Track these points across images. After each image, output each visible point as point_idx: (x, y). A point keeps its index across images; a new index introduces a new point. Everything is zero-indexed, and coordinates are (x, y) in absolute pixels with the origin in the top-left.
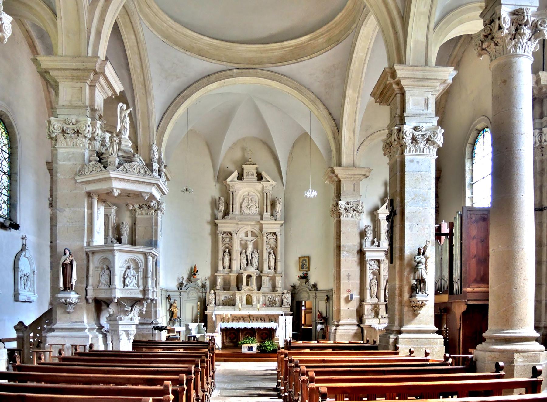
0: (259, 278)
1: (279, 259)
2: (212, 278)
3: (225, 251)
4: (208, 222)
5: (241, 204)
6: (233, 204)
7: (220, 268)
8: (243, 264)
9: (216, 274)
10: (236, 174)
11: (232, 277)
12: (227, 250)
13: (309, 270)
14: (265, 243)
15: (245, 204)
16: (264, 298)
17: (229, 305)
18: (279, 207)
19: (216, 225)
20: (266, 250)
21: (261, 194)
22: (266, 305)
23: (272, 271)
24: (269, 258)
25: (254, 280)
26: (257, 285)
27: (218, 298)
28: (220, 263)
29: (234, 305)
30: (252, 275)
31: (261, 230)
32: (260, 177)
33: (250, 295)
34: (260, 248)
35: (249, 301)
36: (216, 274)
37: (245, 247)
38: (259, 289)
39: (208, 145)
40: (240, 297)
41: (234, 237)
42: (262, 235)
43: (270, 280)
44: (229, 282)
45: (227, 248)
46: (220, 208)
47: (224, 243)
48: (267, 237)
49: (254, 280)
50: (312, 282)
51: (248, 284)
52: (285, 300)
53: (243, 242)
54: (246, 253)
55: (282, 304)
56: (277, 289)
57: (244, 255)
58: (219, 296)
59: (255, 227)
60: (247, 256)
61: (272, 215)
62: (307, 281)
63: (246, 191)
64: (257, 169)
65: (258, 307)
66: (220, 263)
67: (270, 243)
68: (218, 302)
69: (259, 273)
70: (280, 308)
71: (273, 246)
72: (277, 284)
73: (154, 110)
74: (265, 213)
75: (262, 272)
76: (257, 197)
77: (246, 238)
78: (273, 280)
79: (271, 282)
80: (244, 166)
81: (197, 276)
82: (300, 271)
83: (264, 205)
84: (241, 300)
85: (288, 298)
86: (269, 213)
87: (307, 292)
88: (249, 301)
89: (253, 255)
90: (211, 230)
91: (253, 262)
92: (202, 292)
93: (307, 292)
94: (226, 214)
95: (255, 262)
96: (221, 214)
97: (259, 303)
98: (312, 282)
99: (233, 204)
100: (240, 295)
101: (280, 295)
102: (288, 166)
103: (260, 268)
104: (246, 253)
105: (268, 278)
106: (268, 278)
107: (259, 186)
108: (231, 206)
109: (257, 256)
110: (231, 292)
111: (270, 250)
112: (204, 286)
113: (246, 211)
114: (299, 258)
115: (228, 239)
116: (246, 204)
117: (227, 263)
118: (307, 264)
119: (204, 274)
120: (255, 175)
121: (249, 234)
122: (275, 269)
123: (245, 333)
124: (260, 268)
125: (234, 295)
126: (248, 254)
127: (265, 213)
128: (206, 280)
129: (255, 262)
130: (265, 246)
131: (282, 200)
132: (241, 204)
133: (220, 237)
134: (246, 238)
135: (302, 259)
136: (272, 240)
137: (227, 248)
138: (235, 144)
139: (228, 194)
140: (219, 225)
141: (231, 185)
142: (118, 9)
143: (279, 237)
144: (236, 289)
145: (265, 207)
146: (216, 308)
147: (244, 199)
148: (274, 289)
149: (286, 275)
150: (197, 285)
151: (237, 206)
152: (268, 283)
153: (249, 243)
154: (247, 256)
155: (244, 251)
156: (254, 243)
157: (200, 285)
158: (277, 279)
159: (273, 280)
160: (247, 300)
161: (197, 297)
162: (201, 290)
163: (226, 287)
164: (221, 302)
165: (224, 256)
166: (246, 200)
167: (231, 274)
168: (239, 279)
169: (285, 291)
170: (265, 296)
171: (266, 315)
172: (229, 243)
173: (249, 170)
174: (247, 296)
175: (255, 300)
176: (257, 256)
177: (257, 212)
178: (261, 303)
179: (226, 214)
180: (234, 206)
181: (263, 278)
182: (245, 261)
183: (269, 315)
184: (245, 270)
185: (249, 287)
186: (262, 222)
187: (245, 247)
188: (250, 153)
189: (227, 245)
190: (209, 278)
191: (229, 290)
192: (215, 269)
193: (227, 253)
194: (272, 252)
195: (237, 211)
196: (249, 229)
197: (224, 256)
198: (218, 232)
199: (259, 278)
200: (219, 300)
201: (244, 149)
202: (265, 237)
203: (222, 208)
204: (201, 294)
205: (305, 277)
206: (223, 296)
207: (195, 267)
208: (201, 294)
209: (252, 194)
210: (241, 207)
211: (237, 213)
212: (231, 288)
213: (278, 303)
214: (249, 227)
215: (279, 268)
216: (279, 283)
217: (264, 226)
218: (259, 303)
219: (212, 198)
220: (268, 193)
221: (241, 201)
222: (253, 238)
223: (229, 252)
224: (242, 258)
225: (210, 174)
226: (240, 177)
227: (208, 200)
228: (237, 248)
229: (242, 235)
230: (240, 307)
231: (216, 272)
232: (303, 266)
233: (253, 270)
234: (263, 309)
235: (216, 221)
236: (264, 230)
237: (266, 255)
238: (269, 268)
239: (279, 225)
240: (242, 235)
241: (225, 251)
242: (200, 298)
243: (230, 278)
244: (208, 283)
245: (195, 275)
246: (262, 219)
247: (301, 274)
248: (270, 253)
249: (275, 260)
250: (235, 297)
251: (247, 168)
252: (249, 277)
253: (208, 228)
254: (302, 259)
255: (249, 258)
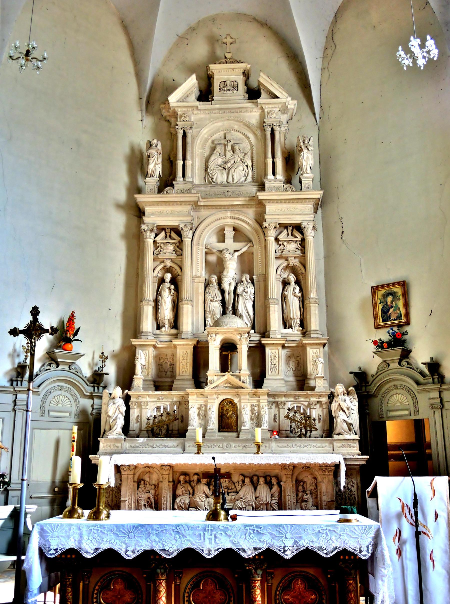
0: (258, 352)
1: (312, 294)
2: (126, 355)
3: (162, 281)
4: (119, 206)
5: (207, 161)
6: (184, 159)
7: (148, 324)
8: (213, 314)
9: (135, 342)
10: (191, 83)
11: (180, 352)
12: (168, 276)
13: (408, 323)
14: (272, 256)
15: (216, 160)
16: (274, 410)
17: (169, 434)
18: (307, 160)
19: (140, 213)
20: (275, 274)
21: (259, 133)
22: (278, 433)
23: (295, 332)
24: (284, 297)
25: (242, 357)
26: (253, 375)
27: (134, 413)
28: (148, 311)
29: (181, 433)
30: (236, 338)
31: (260, 220)
32: (253, 94)
33: (231, 402)
34: (258, 270)
35: (228, 422)
36: (135, 342)
37: (217, 268)
38: (258, 382)
39: (125, 28)
40: (203, 407)
41: (187, 241)
42: (264, 230)
43: (289, 357)
44: (173, 366)
45: (168, 270)
46: (151, 167)
47: (161, 256)
48: (277, 240)
49: (242, 357)
50: (421, 356)
51: (224, 368)
52: (341, 417)
53: (213, 258)
54: (219, 284)
55: (329, 431)
56: (312, 383)
57: (214, 290)
58: (139, 405)
59: (245, 214)
60: (222, 292)
61: (288, 181)
62: (406, 354)
63: (218, 131)
64: (246, 75)
65: (259, 439)
66: (148, 311)
67: (285, 253)
68: (134, 425)
69: (256, 338)
70: (325, 444)
71: (294, 262)
72: (310, 368)
73: (250, 471)
74: (270, 176)
75: (265, 333)
76: (248, 141)
77: (221, 246)
78: (298, 358)
79: (292, 365)
80: (212, 66)
81: (76, 347)
82: (377, 327)
83: (265, 157)
84: (204, 416)
85: (348, 410)
86: (280, 176)
87: (409, 391)
88: (228, 422)
89: (240, 290)
90: (128, 227)
91: (241, 308)
92: (91, 397)
93: (409, 391)
94: (167, 182)
95: (245, 305)
96: (152, 182)
97: (259, 425)
98: (421, 356)
99: (184, 159)
100: (201, 401)
101: (324, 399)
102: (323, 69)
103: (261, 326)
104: (219, 284)
105: (283, 353)
106: (283, 353)
107: (252, 114)
108: (180, 163)
109: (251, 290)
110: (175, 395)
111: (285, 275)
112: (97, 378)
113: (220, 177)
114: (374, 289)
115: (171, 248)
116: (220, 161)
117: (166, 312)
118: (401, 304)
119: (97, 344)
120: (242, 88)
121: (229, 234)
122: (302, 324)
123: (186, 580)
124: (261, 326)
125: (183, 403)
126: (225, 286)
127: (270, 176)
128: (104, 358)
129: (245, 305)
130: (273, 264)
131: (313, 142)
132: (207, 161)
133: (150, 241)
134: (221, 246)
135: (383, 291)
136: (292, 247)
137: (168, 270)
138: (192, 29)
139: (173, 136)
140: (148, 210)
141: (180, 112)
142: (329, 521)
143: (310, 234)
144: (191, 383)
145: (270, 161)
146: (127, 444)
147: (213, 149)
148: (302, 382)
149: (333, 344)
150: (78, 373)
151: (195, 165)
152: (283, 366)
153: (227, 256)
154: (222, 292)
155: (214, 279)
156: (241, 257)
157: (87, 373)
158: (311, 352)
159: (298, 358)
160: (222, 417)
161: (73, 409)
162: (88, 389)
163: (163, 381)
164: (144, 425)
165: (158, 293)
166: (219, 149)
167: (176, 342)
168: (200, 354)
169: (340, 388)
170: (277, 405)
171: (284, 467)
172: (174, 256)
173: (225, 78)
174: (221, 405)
175: (246, 416)
176: (251, 290)
177: (250, 179)
178: (265, 426)
179: (167, 182)
180: (189, 163)
181: (268, 351)
182: (216, 307)
183: (294, 467)
184: (217, 324)
185: (227, 376)
186: (262, 196)
187: (217, 268)
188: (228, 40)
189: (168, 263)
190: (115, 356)
191: (170, 389)
192: (132, 328)
193: (167, 285)
194: (292, 278)
195: (195, 175)
196: (227, 219)
197: (158, 293)
198: (143, 227)
199: (258, 352)
200: (139, 419)
201: (213, 41)
202: (271, 239)
203: (156, 166)
204: (87, 403)
205: (398, 343)
206: (150, 405)
207: (71, 319)
208: (87, 403)
209: (234, 136)
210: (206, 169)
211: (197, 181)
212: (176, 384)
213: (318, 425)
214: (229, 214)
215: (315, 322)
216: (317, 362)
217: (269, 208)
218: (259, 425)
219: (132, 150)
220: (277, 129)
221: (207, 153)
222: (238, 245)
223: (175, 281)
224: (209, 297)
225: (130, 94)
226: (205, 94)
227: (123, 150)
228: (195, 270)
229: (208, 237)
230: (199, 439)
231: (136, 337)
232: (385, 311)
233: (238, 328)
234: (274, 445)
235: (140, 198)
236: (267, 217)
237: (275, 289)
238: (286, 324)
239: (310, 207)
240: (208, 237)
241: (162, 281)
242: (83, 412)
243: (174, 355)
244: (111, 370)
245: (69, 341)
246: (262, 187)
247: (384, 335)
248: (285, 283)
249: (303, 300)
250: (187, 409)
251: (222, 73)
252: (228, 348)
253: (119, 221)
254: (383, 291)
255: (229, 298)
